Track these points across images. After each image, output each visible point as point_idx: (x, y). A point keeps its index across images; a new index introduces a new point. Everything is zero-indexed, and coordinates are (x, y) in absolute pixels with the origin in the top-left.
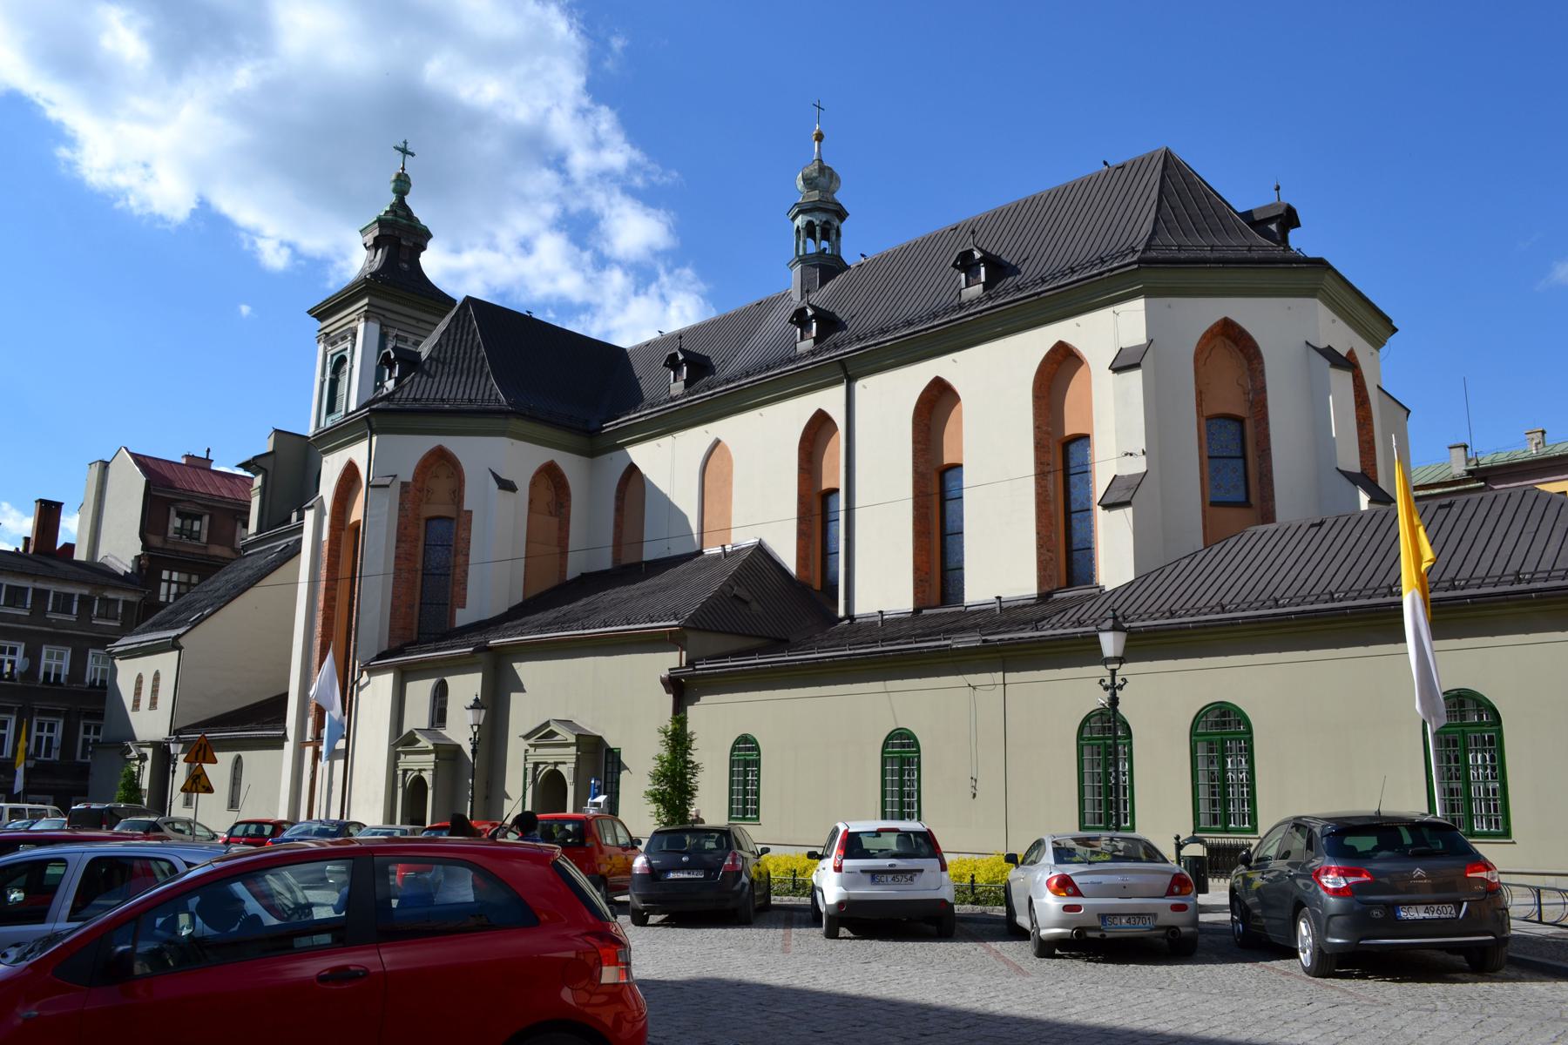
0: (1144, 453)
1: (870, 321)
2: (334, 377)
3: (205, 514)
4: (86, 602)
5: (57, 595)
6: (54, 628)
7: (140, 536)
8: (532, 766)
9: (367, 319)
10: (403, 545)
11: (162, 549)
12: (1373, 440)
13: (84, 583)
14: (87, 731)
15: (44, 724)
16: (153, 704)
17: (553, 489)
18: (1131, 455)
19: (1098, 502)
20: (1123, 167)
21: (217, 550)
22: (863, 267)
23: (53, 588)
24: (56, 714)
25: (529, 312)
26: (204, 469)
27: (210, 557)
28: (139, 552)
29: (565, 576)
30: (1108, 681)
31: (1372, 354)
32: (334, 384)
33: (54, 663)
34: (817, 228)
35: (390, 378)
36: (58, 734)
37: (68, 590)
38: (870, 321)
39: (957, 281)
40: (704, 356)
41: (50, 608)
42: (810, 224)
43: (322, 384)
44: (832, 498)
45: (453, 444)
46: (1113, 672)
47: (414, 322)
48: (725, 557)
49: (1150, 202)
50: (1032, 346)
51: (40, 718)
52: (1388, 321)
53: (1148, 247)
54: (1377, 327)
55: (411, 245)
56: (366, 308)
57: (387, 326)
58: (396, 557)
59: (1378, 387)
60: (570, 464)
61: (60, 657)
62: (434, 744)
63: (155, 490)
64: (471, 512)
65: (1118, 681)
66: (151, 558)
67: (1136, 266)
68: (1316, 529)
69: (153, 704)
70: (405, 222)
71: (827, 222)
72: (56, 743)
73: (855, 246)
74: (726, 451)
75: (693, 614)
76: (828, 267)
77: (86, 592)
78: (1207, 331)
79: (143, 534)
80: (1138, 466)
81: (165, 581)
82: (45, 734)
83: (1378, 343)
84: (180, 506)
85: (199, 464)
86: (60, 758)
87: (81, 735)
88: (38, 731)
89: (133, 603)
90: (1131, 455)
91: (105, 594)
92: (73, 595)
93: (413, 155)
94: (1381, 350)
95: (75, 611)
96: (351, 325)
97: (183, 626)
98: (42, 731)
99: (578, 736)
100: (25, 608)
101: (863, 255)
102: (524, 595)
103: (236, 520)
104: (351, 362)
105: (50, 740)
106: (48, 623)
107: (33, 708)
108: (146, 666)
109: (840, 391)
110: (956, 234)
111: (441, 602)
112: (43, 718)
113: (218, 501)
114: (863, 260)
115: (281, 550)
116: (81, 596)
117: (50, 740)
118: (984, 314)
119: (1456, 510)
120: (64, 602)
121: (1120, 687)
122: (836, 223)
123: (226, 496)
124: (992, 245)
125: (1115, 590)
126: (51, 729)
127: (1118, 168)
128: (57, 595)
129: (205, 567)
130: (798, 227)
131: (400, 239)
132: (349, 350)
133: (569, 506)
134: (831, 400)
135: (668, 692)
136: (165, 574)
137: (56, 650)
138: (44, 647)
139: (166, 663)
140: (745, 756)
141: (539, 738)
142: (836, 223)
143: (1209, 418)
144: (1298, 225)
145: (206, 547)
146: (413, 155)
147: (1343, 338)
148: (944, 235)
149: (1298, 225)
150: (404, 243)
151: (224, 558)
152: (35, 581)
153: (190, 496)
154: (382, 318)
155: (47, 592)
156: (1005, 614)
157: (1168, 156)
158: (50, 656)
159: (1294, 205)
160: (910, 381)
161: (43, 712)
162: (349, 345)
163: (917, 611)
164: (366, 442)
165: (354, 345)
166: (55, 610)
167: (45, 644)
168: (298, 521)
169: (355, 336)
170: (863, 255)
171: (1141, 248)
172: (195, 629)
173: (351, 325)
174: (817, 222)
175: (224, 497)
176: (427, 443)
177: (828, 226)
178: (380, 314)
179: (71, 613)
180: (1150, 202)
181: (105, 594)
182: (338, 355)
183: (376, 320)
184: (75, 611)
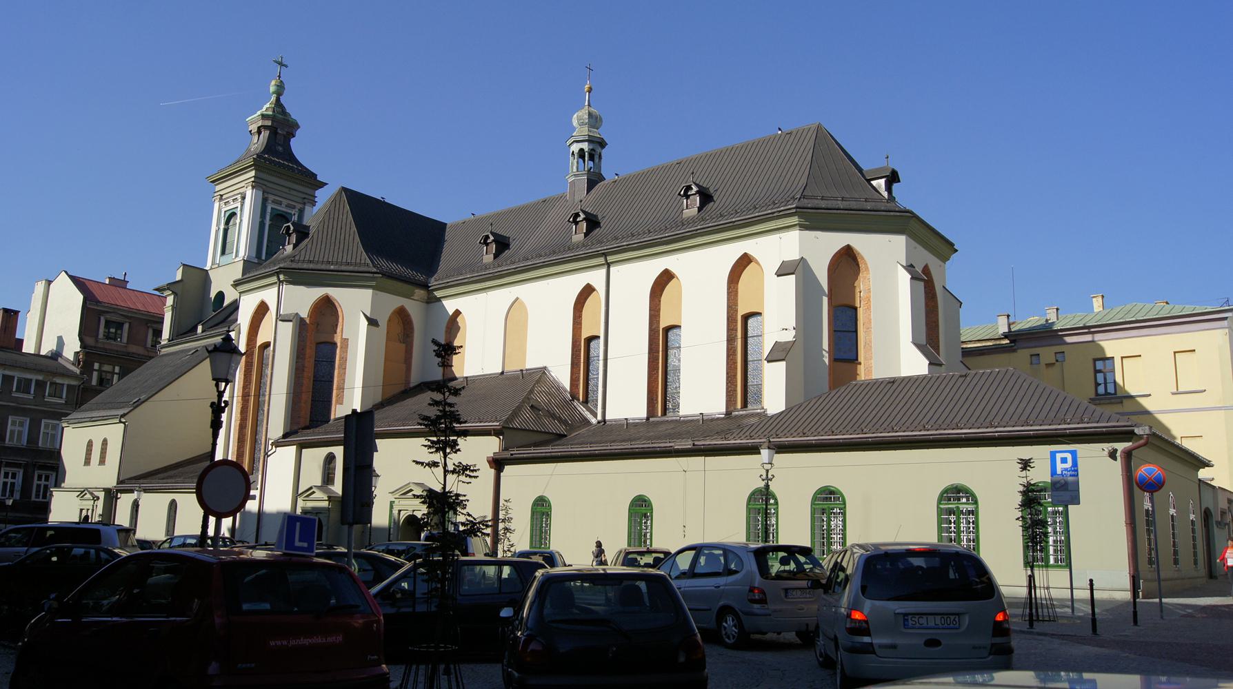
0: (794, 329)
1: (622, 224)
2: (226, 227)
3: (126, 322)
4: (40, 385)
5: (20, 380)
6: (18, 403)
7: (79, 335)
8: (397, 512)
9: (253, 187)
10: (300, 360)
11: (95, 347)
12: (938, 320)
13: (40, 371)
14: (40, 478)
15: (42, 475)
16: (102, 461)
17: (402, 325)
18: (786, 330)
19: (765, 358)
20: (791, 133)
21: (133, 349)
22: (617, 183)
23: (17, 374)
24: (18, 466)
25: (383, 198)
26: (123, 288)
27: (128, 354)
28: (78, 349)
29: (409, 383)
30: (764, 477)
31: (940, 266)
32: (226, 231)
33: (17, 428)
34: (586, 153)
35: (289, 244)
36: (19, 481)
37: (28, 376)
38: (622, 224)
39: (680, 204)
40: (506, 237)
41: (14, 390)
42: (582, 150)
43: (217, 232)
44: (593, 344)
45: (335, 293)
46: (767, 471)
47: (287, 190)
48: (523, 377)
49: (806, 162)
50: (729, 253)
51: (6, 469)
52: (952, 245)
53: (803, 196)
54: (943, 247)
55: (285, 133)
56: (253, 179)
57: (268, 193)
58: (296, 369)
59: (944, 287)
60: (414, 308)
61: (21, 424)
62: (328, 497)
63: (90, 304)
64: (348, 339)
65: (770, 476)
66: (87, 354)
67: (794, 211)
68: (890, 385)
69: (102, 461)
70: (281, 116)
71: (593, 150)
72: (18, 488)
73: (610, 167)
74: (522, 304)
75: (508, 418)
76: (594, 180)
77: (40, 378)
78: (837, 253)
79: (81, 339)
80: (789, 336)
81: (96, 370)
82: (43, 482)
83: (944, 259)
84: (109, 317)
85: (119, 284)
86: (20, 498)
87: (36, 482)
88: (38, 480)
89: (73, 386)
90: (786, 330)
91: (54, 379)
92: (31, 380)
93: (286, 66)
94: (947, 263)
95: (32, 392)
96: (241, 191)
97: (123, 407)
98: (41, 480)
99: (329, 497)
100: (62, 398)
101: (617, 175)
102: (383, 395)
103: (148, 327)
104: (241, 217)
105: (13, 485)
106: (16, 400)
107: (2, 462)
108: (97, 433)
109: (603, 271)
110: (681, 166)
111: (326, 400)
112: (8, 469)
113: (136, 313)
114: (616, 177)
115: (193, 354)
116: (37, 381)
117: (13, 485)
118: (698, 231)
119: (968, 379)
120: (24, 386)
121: (771, 480)
122: (598, 150)
123: (141, 309)
124: (703, 180)
125: (773, 416)
126: (14, 476)
127: (787, 134)
128: (20, 380)
129: (129, 363)
130: (573, 152)
131: (277, 129)
132: (239, 209)
133: (412, 337)
134: (596, 277)
135: (491, 467)
136: (96, 366)
137: (18, 419)
138: (10, 417)
139: (113, 433)
140: (541, 509)
141: (305, 497)
142: (598, 150)
143: (835, 307)
144: (899, 181)
145: (126, 347)
146: (286, 66)
147: (925, 257)
148: (672, 167)
149: (899, 181)
150: (280, 132)
151: (139, 355)
152: (5, 369)
153: (115, 310)
154: (264, 187)
155: (13, 377)
156: (704, 424)
157: (819, 127)
158: (14, 423)
159: (896, 169)
160: (649, 269)
161: (8, 465)
162: (239, 205)
163: (648, 419)
164: (277, 288)
165: (242, 205)
166: (18, 390)
167: (11, 415)
168: (202, 332)
169: (243, 198)
170: (617, 175)
171: (798, 196)
172: (136, 410)
173: (241, 191)
174: (586, 150)
175: (139, 310)
176: (317, 293)
177: (593, 153)
178: (263, 184)
179: (62, 398)
180: (806, 162)
181: (54, 379)
182: (231, 211)
183: (260, 189)
184: (32, 392)
